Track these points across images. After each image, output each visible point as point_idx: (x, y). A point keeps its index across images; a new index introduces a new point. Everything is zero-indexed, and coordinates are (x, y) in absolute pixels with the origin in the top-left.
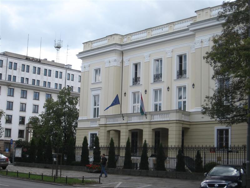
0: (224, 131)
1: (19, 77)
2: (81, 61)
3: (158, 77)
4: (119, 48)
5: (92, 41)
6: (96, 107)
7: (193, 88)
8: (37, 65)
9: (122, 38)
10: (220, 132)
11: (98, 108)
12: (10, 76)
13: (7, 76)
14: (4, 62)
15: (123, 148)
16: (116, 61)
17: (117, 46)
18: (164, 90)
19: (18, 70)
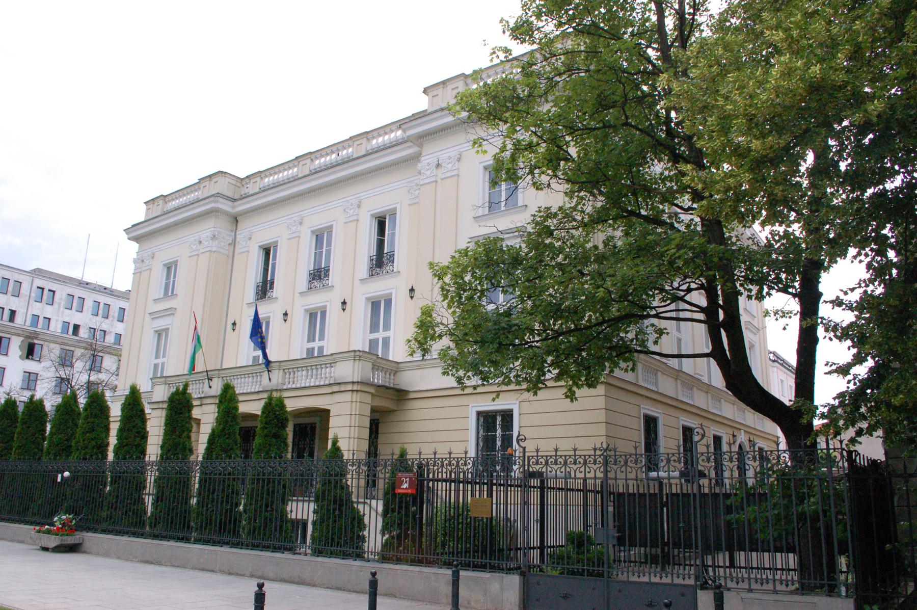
0: (499, 419)
1: (57, 320)
2: (135, 246)
3: (319, 275)
4: (226, 206)
5: (165, 196)
6: (159, 361)
7: (412, 297)
8: (104, 299)
9: (238, 184)
10: (487, 420)
11: (163, 364)
12: (36, 317)
13: (29, 317)
14: (23, 286)
15: (152, 464)
16: (217, 239)
17: (220, 199)
18: (333, 311)
19: (56, 306)
